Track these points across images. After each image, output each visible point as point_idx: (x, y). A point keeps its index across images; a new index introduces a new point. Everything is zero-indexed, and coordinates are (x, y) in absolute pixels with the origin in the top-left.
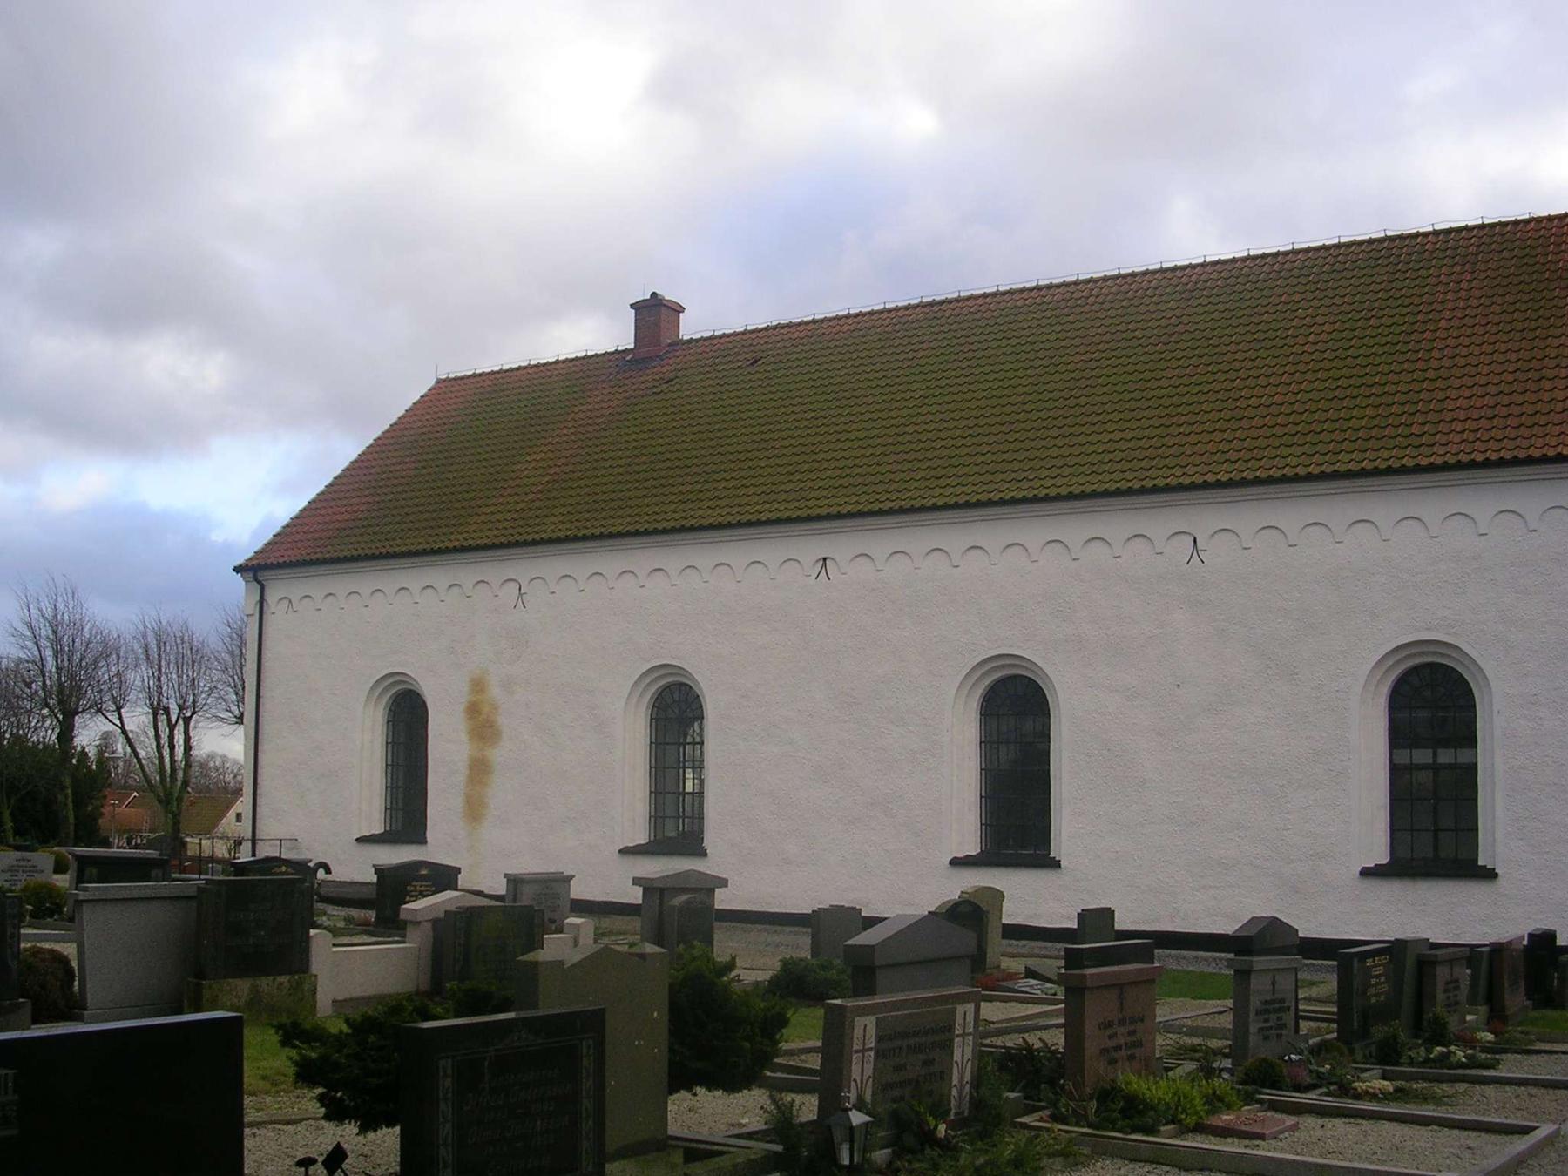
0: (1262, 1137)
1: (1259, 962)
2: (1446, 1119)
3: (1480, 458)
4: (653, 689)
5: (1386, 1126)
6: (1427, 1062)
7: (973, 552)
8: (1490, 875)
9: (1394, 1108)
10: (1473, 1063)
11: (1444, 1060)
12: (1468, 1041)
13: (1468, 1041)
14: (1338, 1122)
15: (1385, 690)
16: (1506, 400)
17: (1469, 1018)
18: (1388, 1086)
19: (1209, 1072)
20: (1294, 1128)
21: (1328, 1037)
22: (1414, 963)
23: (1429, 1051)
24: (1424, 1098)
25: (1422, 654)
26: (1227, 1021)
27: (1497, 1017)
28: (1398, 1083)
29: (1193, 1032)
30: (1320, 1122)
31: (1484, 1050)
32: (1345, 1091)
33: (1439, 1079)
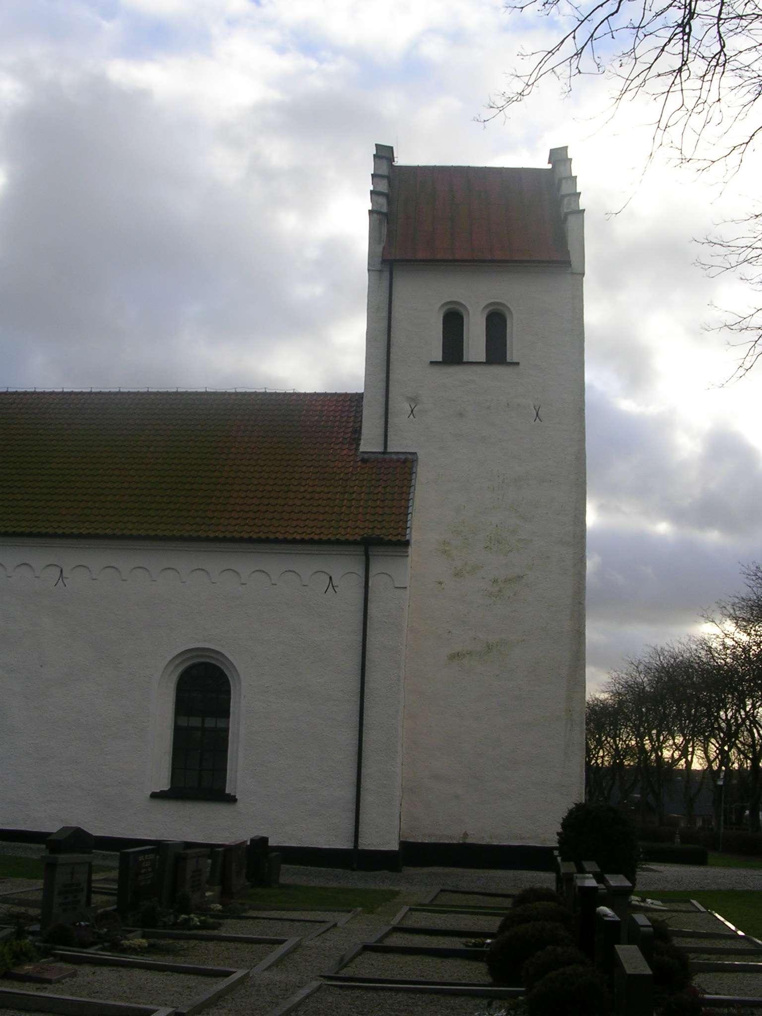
0: (49, 981)
1: (62, 858)
2: (176, 967)
3: (246, 536)
4: (196, 661)
5: (137, 972)
6: (175, 925)
7: (108, 570)
8: (232, 800)
9: (148, 959)
10: (204, 926)
11: (186, 924)
12: (202, 910)
13: (202, 910)
14: (105, 970)
15: (175, 678)
16: (266, 502)
17: (208, 894)
18: (144, 942)
19: (20, 934)
20: (74, 975)
21: (108, 909)
22: (171, 858)
23: (177, 917)
24: (167, 951)
25: (202, 656)
26: (39, 896)
27: (226, 893)
28: (152, 941)
29: (21, 903)
30: (93, 969)
31: (212, 916)
32: (116, 947)
33: (178, 938)
